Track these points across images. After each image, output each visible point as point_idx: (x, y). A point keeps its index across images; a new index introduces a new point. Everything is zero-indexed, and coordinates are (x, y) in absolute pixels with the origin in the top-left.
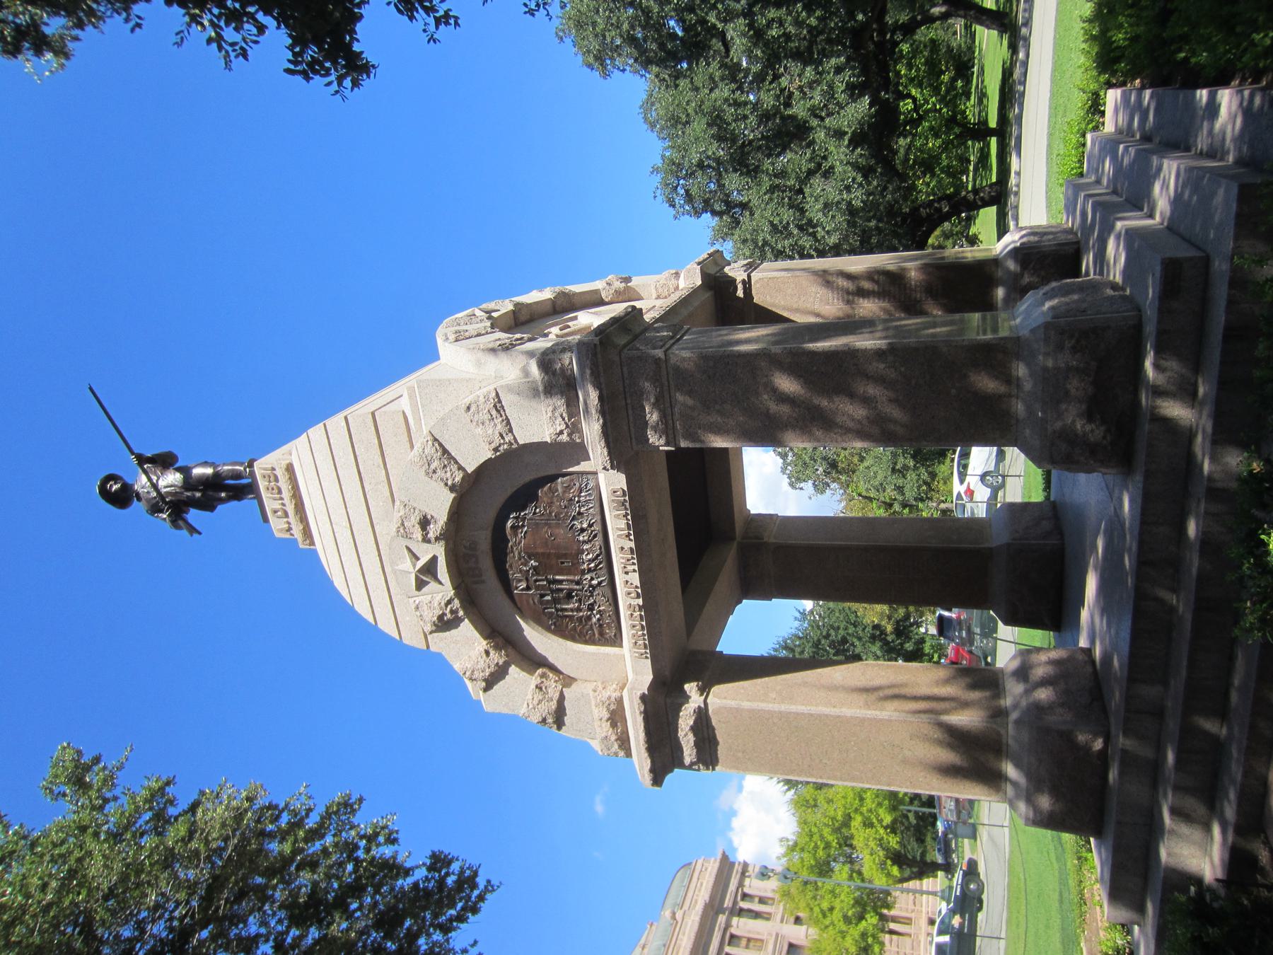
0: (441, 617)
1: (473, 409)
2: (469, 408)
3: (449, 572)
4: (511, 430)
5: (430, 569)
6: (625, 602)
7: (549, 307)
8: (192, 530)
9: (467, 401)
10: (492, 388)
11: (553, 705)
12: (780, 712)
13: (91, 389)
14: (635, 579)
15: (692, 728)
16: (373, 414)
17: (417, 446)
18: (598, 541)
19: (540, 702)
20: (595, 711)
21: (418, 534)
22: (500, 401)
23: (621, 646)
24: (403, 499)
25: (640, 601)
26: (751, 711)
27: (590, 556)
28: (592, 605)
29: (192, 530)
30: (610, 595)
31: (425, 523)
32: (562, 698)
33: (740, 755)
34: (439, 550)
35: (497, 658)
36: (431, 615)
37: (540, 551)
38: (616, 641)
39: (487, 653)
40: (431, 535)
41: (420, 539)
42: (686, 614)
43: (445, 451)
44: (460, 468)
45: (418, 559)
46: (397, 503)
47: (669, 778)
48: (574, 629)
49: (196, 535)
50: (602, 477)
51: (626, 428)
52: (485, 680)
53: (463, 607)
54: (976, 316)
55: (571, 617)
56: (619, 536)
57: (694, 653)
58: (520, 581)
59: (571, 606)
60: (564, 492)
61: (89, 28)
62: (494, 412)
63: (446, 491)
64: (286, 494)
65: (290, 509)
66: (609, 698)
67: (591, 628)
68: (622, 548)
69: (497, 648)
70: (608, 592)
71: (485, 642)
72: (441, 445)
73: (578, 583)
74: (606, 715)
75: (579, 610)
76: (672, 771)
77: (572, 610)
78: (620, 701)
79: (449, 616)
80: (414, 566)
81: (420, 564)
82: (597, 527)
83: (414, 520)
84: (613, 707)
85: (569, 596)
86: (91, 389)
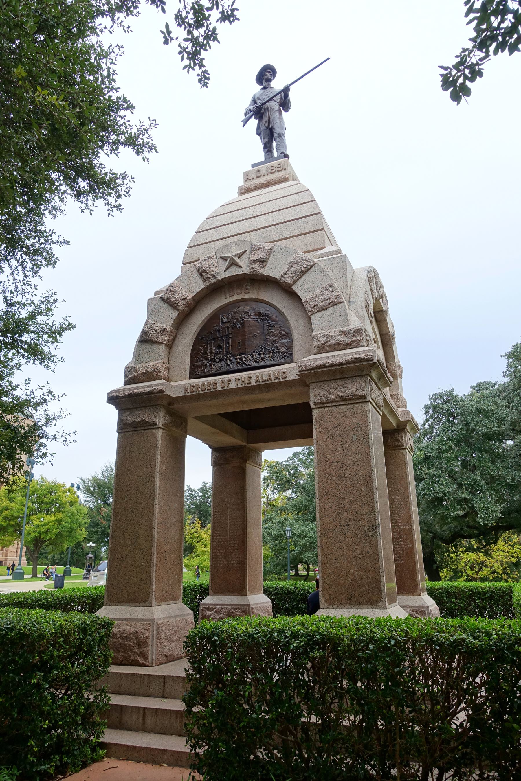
0: (204, 271)
1: (331, 289)
2: (331, 286)
3: (232, 276)
4: (318, 311)
5: (233, 263)
6: (218, 380)
7: (384, 331)
8: (245, 122)
9: (335, 285)
10: (344, 300)
11: (154, 339)
12: (154, 472)
13: (328, 59)
14: (233, 386)
15: (143, 420)
16: (323, 229)
17: (305, 255)
18: (252, 363)
19: (156, 331)
20: (151, 364)
21: (253, 258)
22: (336, 304)
23: (190, 378)
24: (275, 249)
25: (219, 389)
26: (155, 455)
27: (244, 359)
28: (215, 361)
29: (245, 122)
30: (221, 371)
31: (262, 261)
32: (160, 343)
33: (128, 449)
34: (245, 270)
35: (182, 305)
36: (206, 265)
37: (247, 329)
38: (193, 376)
39: (185, 299)
40: (254, 266)
41: (251, 259)
42: (207, 416)
43: (304, 272)
44: (295, 282)
45: (239, 257)
46: (272, 245)
47: (112, 408)
48: (200, 350)
49: (242, 124)
50: (293, 365)
51: (323, 379)
52: (168, 299)
53: (211, 285)
54: (395, 585)
55: (207, 348)
56: (257, 377)
57: (185, 421)
58: (227, 318)
59: (214, 349)
60: (282, 344)
61: (474, 34)
62: (329, 301)
63: (281, 274)
64: (270, 177)
65: (262, 180)
66: (160, 372)
67: (200, 361)
68: (250, 378)
69: (188, 305)
70: (224, 370)
71: (190, 298)
72: (309, 270)
73: (227, 352)
74: (150, 369)
75: (211, 353)
76: (117, 409)
77: (211, 349)
78: (158, 378)
79: (206, 277)
80: (235, 256)
81: (236, 259)
82: (263, 363)
83: (262, 254)
84: (154, 374)
85: (220, 347)
86: (328, 59)
